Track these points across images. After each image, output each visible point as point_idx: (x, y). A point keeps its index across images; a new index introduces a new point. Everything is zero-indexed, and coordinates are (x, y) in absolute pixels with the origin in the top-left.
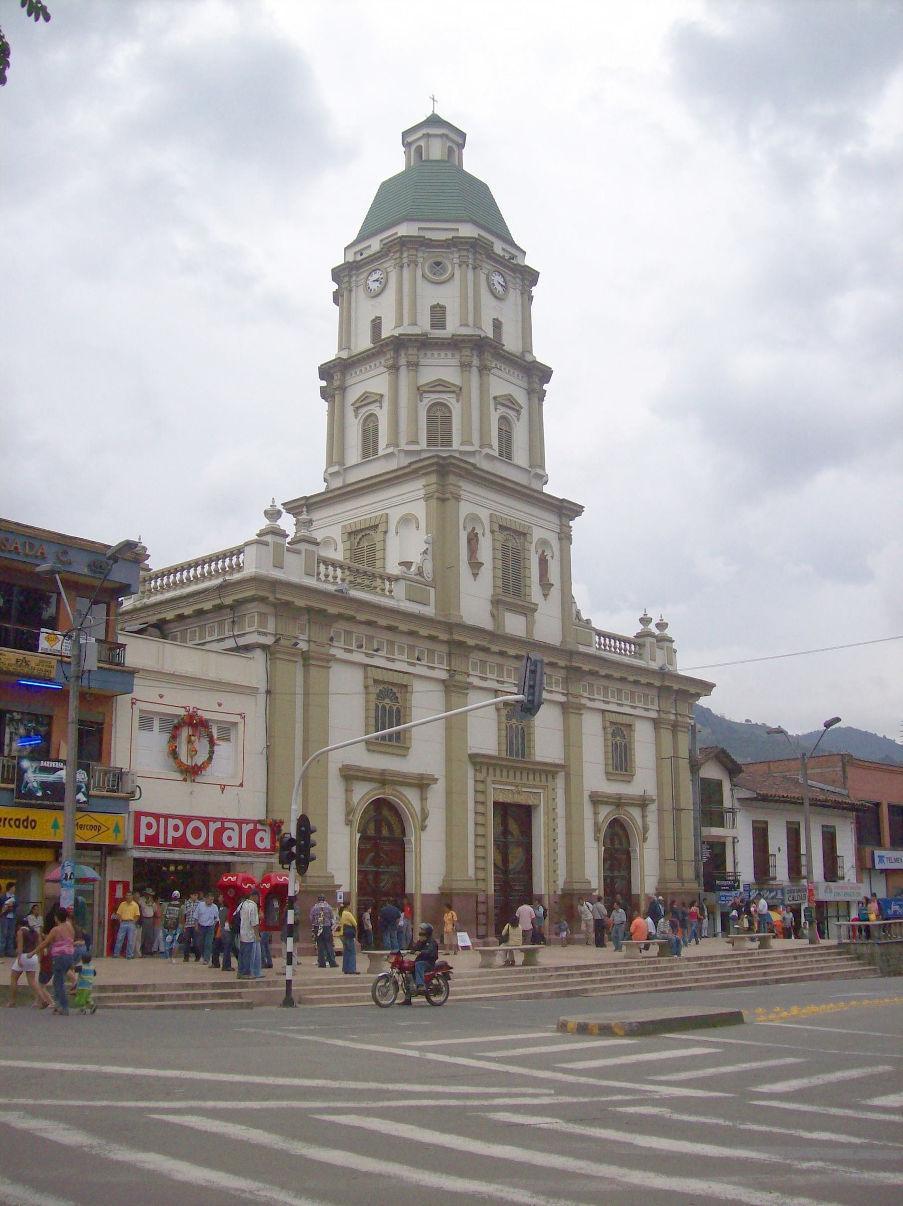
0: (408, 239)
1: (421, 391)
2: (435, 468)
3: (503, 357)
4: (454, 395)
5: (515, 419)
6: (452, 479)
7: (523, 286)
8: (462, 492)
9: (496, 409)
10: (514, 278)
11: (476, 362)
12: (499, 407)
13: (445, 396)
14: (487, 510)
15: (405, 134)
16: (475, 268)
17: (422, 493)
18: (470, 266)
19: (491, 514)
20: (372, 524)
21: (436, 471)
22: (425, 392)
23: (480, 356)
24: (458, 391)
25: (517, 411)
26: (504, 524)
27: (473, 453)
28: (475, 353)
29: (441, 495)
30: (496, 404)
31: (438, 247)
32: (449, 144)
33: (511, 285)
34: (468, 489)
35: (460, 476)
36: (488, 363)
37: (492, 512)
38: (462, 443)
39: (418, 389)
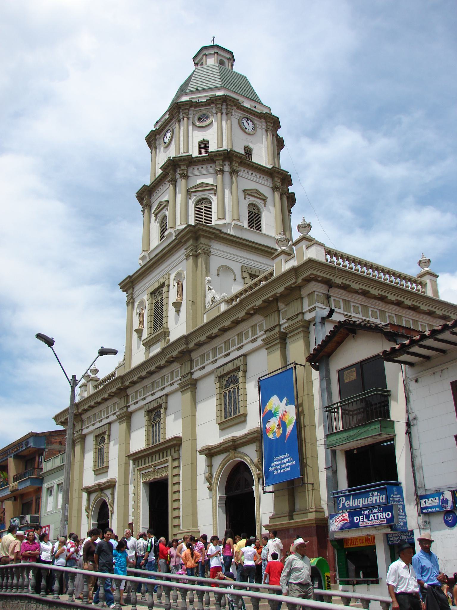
0: (181, 103)
1: (189, 193)
2: (301, 329)
3: (252, 166)
4: (212, 192)
5: (263, 205)
6: (202, 240)
7: (266, 126)
8: (211, 250)
9: (245, 198)
10: (261, 122)
11: (227, 168)
12: (247, 196)
13: (206, 193)
14: (241, 263)
15: (194, 59)
16: (227, 114)
17: (184, 257)
18: (224, 114)
19: (242, 266)
20: (235, 367)
21: (303, 331)
22: (192, 192)
23: (231, 165)
24: (214, 189)
25: (263, 200)
26: (254, 273)
27: (225, 225)
28: (227, 163)
29: (195, 253)
30: (245, 196)
31: (202, 106)
32: (220, 58)
33: (258, 126)
34: (217, 247)
35: (210, 238)
36: (235, 168)
37: (242, 264)
38: (219, 219)
39: (188, 191)
